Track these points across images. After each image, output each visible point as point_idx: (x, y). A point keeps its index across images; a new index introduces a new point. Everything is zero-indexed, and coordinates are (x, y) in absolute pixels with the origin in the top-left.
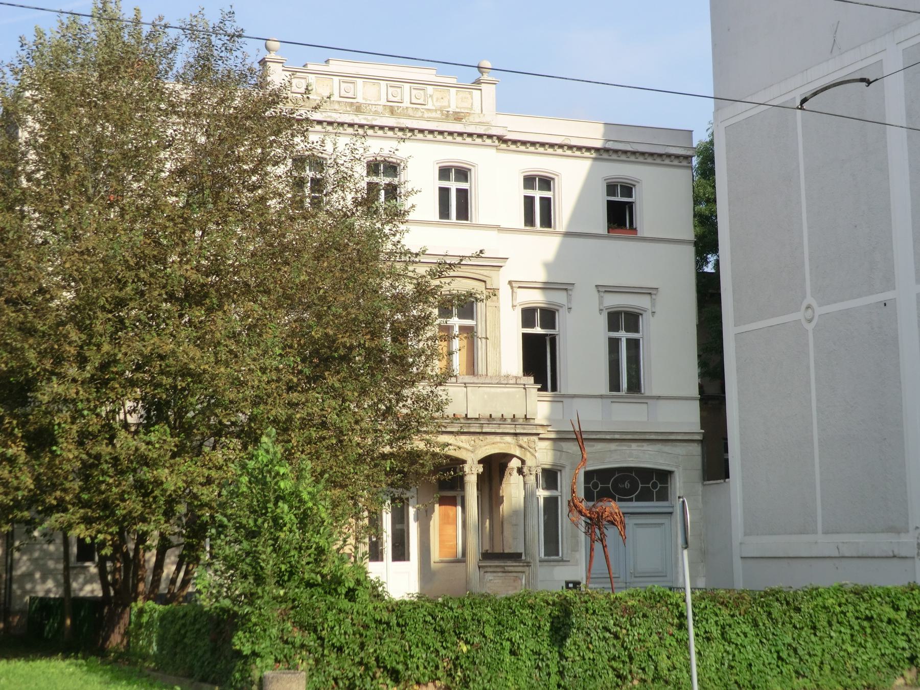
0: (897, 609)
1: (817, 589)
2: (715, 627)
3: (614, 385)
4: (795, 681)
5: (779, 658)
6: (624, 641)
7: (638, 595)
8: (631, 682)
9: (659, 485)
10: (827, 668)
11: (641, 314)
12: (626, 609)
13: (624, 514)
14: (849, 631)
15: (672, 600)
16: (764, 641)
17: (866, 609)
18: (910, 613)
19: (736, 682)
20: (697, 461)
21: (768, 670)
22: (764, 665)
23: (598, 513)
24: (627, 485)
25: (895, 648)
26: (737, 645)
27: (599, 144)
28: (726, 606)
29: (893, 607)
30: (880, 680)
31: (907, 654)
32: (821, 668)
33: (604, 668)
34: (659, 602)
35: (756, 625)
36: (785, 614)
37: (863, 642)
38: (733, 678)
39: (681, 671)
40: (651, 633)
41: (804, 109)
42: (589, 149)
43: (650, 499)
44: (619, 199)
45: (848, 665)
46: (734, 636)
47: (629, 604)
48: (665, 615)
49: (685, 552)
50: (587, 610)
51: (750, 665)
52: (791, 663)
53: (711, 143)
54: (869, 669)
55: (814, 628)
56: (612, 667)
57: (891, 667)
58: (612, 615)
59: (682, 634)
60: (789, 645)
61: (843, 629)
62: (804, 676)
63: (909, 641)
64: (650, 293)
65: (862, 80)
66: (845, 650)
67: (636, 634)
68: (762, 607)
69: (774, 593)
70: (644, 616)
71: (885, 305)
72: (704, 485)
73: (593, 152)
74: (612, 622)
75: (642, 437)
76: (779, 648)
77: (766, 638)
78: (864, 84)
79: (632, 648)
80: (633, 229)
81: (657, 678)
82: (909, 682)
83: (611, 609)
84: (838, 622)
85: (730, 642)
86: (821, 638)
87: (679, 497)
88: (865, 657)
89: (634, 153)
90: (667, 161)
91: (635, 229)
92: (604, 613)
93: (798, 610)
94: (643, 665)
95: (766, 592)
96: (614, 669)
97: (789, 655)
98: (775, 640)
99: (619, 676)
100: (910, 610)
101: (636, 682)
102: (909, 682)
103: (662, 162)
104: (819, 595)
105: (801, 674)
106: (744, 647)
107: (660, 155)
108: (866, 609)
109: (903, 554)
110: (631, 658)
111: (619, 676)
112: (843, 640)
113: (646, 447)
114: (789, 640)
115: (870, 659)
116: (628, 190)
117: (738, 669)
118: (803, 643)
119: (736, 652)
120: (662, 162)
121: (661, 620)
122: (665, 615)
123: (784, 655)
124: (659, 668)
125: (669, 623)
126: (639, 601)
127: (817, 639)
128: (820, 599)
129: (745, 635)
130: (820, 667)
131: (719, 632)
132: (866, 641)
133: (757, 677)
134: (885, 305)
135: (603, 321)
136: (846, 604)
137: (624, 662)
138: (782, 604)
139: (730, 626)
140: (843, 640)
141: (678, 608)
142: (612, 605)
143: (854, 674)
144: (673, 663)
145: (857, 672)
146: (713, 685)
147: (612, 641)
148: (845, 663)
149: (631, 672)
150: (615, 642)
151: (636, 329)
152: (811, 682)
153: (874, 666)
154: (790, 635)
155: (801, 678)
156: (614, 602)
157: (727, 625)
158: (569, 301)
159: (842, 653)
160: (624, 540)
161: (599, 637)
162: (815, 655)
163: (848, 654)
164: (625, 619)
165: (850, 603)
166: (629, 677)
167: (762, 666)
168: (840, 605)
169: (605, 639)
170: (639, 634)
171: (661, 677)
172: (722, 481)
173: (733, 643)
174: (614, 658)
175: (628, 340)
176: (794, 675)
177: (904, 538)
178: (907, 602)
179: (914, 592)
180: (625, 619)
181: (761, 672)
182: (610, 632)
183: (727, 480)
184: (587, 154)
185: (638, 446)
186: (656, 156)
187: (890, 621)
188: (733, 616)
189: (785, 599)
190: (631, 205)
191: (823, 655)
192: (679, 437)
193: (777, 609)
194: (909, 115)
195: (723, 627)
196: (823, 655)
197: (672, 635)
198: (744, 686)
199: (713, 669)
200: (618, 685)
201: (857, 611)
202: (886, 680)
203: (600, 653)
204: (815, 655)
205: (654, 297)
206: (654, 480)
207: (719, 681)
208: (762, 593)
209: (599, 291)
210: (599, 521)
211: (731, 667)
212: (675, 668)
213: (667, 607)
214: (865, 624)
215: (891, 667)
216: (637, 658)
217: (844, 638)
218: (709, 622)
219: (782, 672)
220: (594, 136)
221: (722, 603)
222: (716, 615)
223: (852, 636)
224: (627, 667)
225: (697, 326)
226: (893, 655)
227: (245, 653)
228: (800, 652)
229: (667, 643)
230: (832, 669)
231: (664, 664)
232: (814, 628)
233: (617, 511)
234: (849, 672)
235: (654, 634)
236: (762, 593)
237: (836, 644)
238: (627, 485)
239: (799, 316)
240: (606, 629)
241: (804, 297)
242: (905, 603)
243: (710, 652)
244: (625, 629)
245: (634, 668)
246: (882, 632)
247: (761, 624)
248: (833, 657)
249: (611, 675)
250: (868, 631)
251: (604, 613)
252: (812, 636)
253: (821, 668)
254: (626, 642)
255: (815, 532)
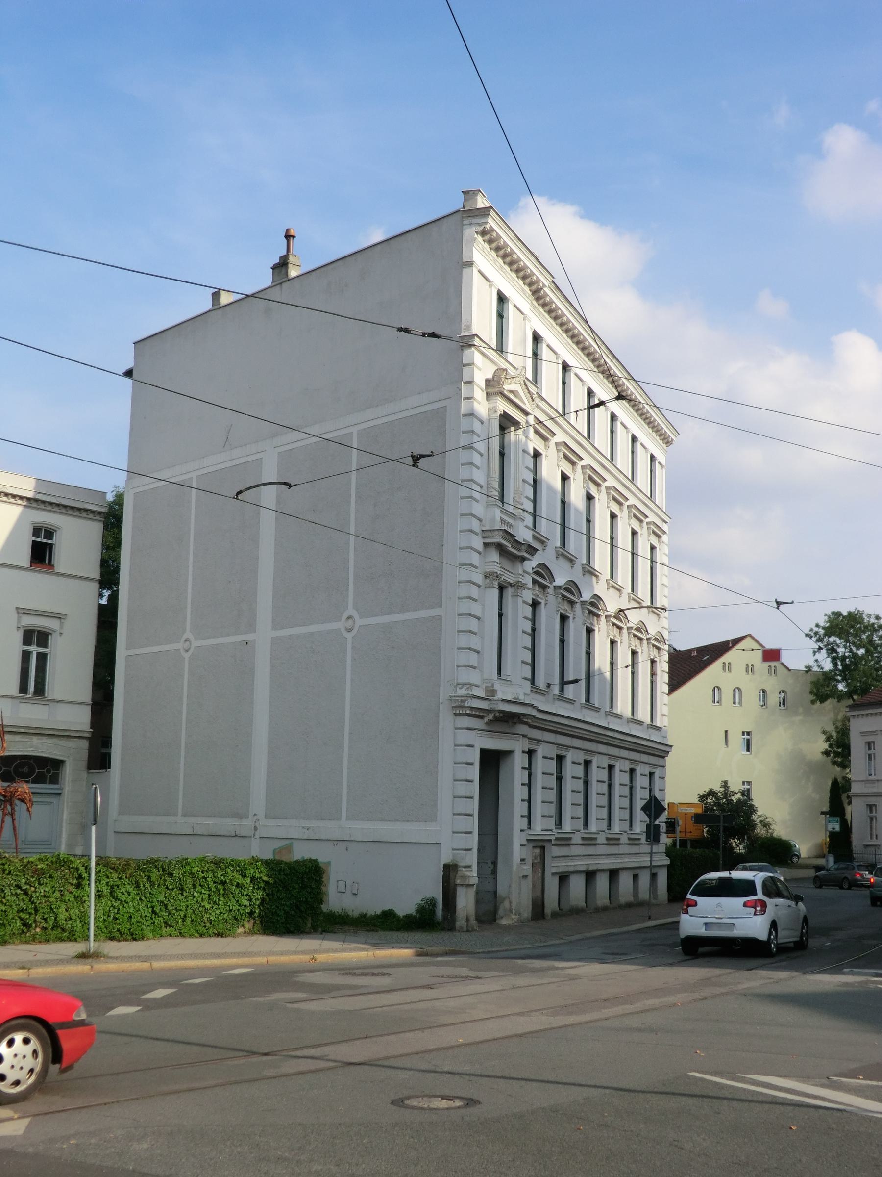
0: (244, 876)
1: (186, 859)
2: (106, 887)
3: (23, 689)
4: (164, 930)
5: (154, 912)
6: (32, 897)
7: (47, 860)
8: (35, 930)
9: (4, 769)
10: (188, 920)
11: (51, 634)
12: (36, 871)
13: (32, 793)
14: (207, 892)
15: (74, 865)
16: (143, 898)
17: (222, 875)
18: (253, 879)
19: (118, 930)
20: (85, 754)
21: (144, 921)
22: (141, 917)
23: (11, 792)
24: (26, 770)
25: (240, 905)
26: (121, 901)
27: (30, 495)
28: (115, 870)
29: (241, 875)
30: (227, 929)
31: (248, 910)
32: (184, 921)
33: (13, 918)
34: (63, 866)
35: (138, 886)
36: (161, 878)
37: (217, 900)
38: (117, 927)
39: (76, 921)
40: (55, 891)
41: (239, 499)
42: (21, 498)
43: (44, 782)
44: (42, 540)
45: (204, 918)
46: (120, 894)
47: (39, 866)
48: (67, 876)
49: (94, 828)
50: (4, 871)
51: (131, 917)
52: (162, 916)
53: (572, 607)
54: (219, 921)
55: (182, 889)
56: (20, 917)
57: (236, 919)
58: (24, 875)
59: (79, 892)
60: (162, 902)
61: (203, 891)
62: (170, 926)
63: (250, 900)
64: (60, 618)
65: (285, 484)
66: (204, 907)
67: (42, 891)
68: (144, 872)
69: (153, 862)
70: (50, 877)
71: (247, 643)
72: (89, 773)
73: (24, 500)
74: (24, 881)
75: (42, 732)
76: (154, 904)
77: (144, 896)
78: (287, 486)
79: (38, 902)
80: (51, 565)
81: (56, 926)
82: (247, 930)
83: (24, 871)
84: (200, 885)
85: (116, 899)
86: (186, 897)
87: (93, 784)
88: (217, 912)
89: (58, 505)
90: (84, 515)
91: (53, 565)
92: (18, 873)
93: (171, 875)
94: (46, 916)
95: (147, 861)
96: (21, 919)
97: (160, 909)
98: (152, 898)
99: (25, 924)
100: (254, 877)
101: (38, 930)
102: (247, 930)
103: (80, 515)
104: (188, 864)
105: (169, 925)
106: (127, 903)
107: (79, 509)
108: (222, 875)
109: (243, 835)
110: (36, 910)
111: (25, 924)
112: (202, 898)
113: (45, 740)
114: (161, 898)
115: (221, 913)
116: (49, 534)
117: (121, 920)
118: (172, 901)
119: (121, 907)
120: (80, 515)
121: (63, 880)
122: (67, 876)
123: (157, 909)
124: (58, 919)
125: (70, 883)
126: (47, 864)
127: (183, 897)
128: (188, 867)
129: (129, 893)
130: (183, 919)
131: (108, 891)
132: (219, 900)
133: (135, 926)
134: (247, 643)
135: (19, 636)
136: (207, 871)
137: (30, 914)
138: (159, 870)
139: (118, 887)
140: (202, 898)
141: (78, 872)
142: (25, 867)
143: (208, 925)
144: (70, 914)
145: (211, 923)
146: (100, 932)
147: (22, 897)
148: (203, 916)
149: (35, 921)
150: (24, 897)
151: (45, 645)
152: (176, 930)
153: (224, 919)
154: (163, 893)
155: (168, 928)
156: (27, 865)
157: (116, 886)
158: (61, 627)
159: (201, 909)
160: (30, 815)
161: (12, 894)
162: (180, 910)
163: (205, 909)
164: (34, 879)
165: (210, 871)
166: (34, 925)
167: (139, 918)
168: (203, 872)
169: (17, 895)
170: (45, 891)
171: (59, 926)
172: (104, 771)
173: (119, 900)
174: (22, 911)
175: (38, 654)
176: (163, 925)
177: (245, 822)
178: (252, 871)
179: (257, 863)
180: (34, 879)
181: (138, 922)
182: (22, 890)
183: (108, 770)
184: (20, 502)
185: (38, 739)
186: (47, 504)
187: (238, 885)
188: (120, 879)
189: (162, 867)
190: (51, 547)
191: (186, 910)
192: (72, 734)
193: (155, 874)
194: (278, 502)
195: (112, 887)
196: (186, 910)
197: (71, 892)
198: (124, 933)
199: (101, 919)
200: (23, 932)
201: (215, 877)
202: (231, 929)
203: (11, 906)
204: (180, 910)
205: (63, 621)
206: (49, 767)
207: (105, 929)
208: (145, 861)
209: (18, 612)
210: (11, 798)
211: (115, 919)
212: (71, 919)
213: (69, 870)
214: (220, 887)
215: (236, 919)
216: (41, 911)
217: (204, 897)
218: (102, 883)
219: (154, 923)
220: (27, 487)
221: (113, 869)
222: (108, 877)
223: (210, 895)
224: (32, 918)
225: (96, 647)
226: (238, 910)
227: (322, 906)
228: (170, 907)
229: (67, 898)
230: (192, 921)
231: (63, 915)
232: (182, 889)
233: (27, 791)
234: (205, 923)
235: (57, 892)
236: (145, 861)
237: (197, 902)
238: (26, 770)
239: (180, 646)
240: (18, 887)
241: (184, 632)
242: (251, 871)
243: (100, 906)
244: (34, 887)
245: (38, 919)
246: (232, 893)
247: (142, 886)
248: (194, 912)
249: (18, 924)
250: (222, 892)
251: (18, 873)
252: (180, 895)
253: (184, 921)
254: (33, 897)
255: (176, 815)
